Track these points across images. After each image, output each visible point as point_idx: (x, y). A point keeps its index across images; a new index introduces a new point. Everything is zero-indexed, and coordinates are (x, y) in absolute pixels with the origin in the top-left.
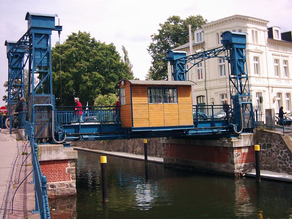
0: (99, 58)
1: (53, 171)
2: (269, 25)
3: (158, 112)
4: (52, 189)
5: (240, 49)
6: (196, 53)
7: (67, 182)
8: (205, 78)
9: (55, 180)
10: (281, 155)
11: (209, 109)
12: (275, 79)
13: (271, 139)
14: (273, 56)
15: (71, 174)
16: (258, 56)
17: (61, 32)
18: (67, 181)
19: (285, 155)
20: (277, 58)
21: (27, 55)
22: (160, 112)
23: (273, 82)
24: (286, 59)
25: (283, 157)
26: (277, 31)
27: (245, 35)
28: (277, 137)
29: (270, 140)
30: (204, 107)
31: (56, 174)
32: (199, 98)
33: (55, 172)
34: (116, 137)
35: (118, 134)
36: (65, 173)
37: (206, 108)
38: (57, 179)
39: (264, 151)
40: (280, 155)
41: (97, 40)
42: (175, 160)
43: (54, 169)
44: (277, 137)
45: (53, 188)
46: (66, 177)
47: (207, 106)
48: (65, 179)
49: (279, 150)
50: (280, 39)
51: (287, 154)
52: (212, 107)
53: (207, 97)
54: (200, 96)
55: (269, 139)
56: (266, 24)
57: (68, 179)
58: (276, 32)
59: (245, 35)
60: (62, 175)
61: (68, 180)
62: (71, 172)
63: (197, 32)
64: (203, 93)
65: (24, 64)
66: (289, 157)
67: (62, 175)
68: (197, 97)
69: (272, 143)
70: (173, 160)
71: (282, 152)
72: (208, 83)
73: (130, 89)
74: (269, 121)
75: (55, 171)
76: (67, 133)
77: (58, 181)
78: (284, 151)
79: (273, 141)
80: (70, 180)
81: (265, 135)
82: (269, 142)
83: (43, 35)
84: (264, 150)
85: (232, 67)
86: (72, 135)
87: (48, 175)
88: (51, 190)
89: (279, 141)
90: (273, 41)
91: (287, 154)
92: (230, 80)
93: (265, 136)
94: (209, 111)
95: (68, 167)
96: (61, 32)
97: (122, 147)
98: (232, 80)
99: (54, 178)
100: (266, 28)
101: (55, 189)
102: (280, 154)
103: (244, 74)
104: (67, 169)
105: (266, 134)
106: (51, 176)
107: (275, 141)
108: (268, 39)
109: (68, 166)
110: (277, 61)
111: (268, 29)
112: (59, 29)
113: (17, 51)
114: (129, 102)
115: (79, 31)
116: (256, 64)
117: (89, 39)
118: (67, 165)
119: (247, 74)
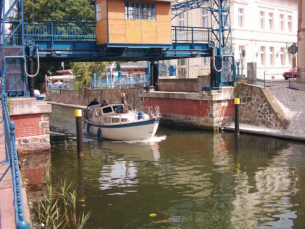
0: (75, 8)
4: (25, 144)
7: (40, 137)
10: (261, 108)
15: (45, 129)
18: (41, 136)
19: (265, 108)
25: (263, 111)
36: (39, 128)
39: (244, 105)
40: (259, 109)
43: (27, 123)
45: (26, 142)
46: (40, 131)
48: (38, 133)
49: (259, 104)
51: (267, 108)
55: (250, 93)
57: (41, 133)
60: (35, 130)
61: (42, 135)
62: (44, 126)
67: (35, 130)
71: (262, 106)
77: (31, 136)
80: (44, 134)
81: (246, 88)
84: (244, 103)
87: (20, 130)
88: (24, 145)
89: (259, 95)
91: (267, 108)
95: (41, 122)
99: (27, 132)
101: (28, 144)
102: (260, 107)
104: (40, 123)
105: (247, 87)
107: (255, 95)
109: (42, 120)
110: (262, 13)
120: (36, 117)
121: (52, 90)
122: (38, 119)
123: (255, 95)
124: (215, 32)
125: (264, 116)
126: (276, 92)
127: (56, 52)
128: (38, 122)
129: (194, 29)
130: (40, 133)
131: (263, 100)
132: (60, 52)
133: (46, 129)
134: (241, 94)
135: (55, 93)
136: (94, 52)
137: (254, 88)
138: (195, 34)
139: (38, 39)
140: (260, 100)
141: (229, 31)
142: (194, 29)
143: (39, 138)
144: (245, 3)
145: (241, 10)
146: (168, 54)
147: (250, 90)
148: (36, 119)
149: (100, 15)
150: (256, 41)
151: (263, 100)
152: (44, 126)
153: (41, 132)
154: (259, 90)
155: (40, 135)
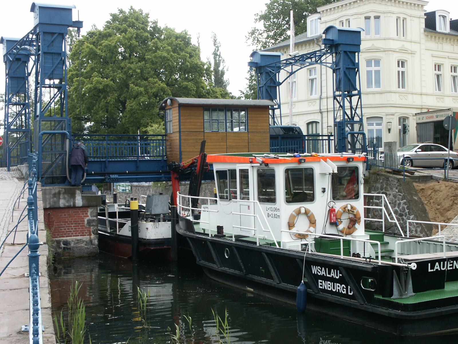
0: (165, 54)
1: (67, 222)
2: (429, 9)
3: (218, 144)
5: (350, 52)
7: (86, 238)
8: (320, 94)
9: (69, 234)
10: (399, 208)
11: (324, 141)
12: (435, 96)
13: (387, 185)
15: (92, 227)
16: (406, 59)
17: (81, 29)
19: (403, 208)
20: (439, 61)
21: (34, 59)
22: (222, 144)
25: (400, 211)
26: (444, 17)
27: (360, 32)
28: (395, 181)
29: (386, 188)
30: (318, 138)
31: (71, 226)
32: (310, 126)
33: (69, 224)
34: (159, 177)
35: (161, 174)
36: (84, 226)
37: (321, 139)
38: (73, 234)
39: (378, 203)
40: (397, 208)
41: (161, 25)
43: (69, 219)
44: (395, 181)
46: (85, 231)
47: (322, 136)
48: (84, 233)
49: (395, 202)
50: (448, 30)
51: (406, 206)
52: (329, 138)
53: (322, 123)
54: (312, 123)
55: (385, 186)
56: (422, 6)
58: (442, 18)
59: (360, 32)
60: (80, 228)
62: (92, 224)
63: (311, 19)
64: (317, 118)
65: (29, 71)
66: (407, 211)
67: (80, 228)
68: (308, 124)
69: (388, 191)
71: (399, 204)
73: (178, 111)
74: (389, 160)
75: (70, 222)
76: (87, 170)
77: (74, 236)
78: (401, 202)
79: (389, 189)
81: (380, 180)
82: (385, 190)
83: (56, 35)
84: (377, 201)
85: (338, 80)
86: (96, 174)
89: (397, 189)
90: (437, 35)
91: (406, 206)
92: (335, 98)
93: (379, 181)
94: (324, 144)
95: (88, 218)
96: (81, 29)
98: (338, 98)
100: (423, 14)
102: (397, 206)
103: (355, 89)
104: (86, 220)
105: (382, 178)
106: (64, 229)
107: (392, 189)
108: (425, 31)
109: (88, 216)
110: (438, 67)
112: (79, 25)
113: (19, 53)
114: (177, 128)
115: (131, 7)
117: (148, 22)
118: (87, 214)
119: (359, 90)
120: (81, 212)
121: (119, 186)
122: (83, 214)
123: (392, 189)
124: (338, 98)
125: (402, 219)
128: (83, 219)
130: (86, 233)
131: (401, 196)
133: (93, 228)
134: (374, 188)
135: (123, 190)
137: (390, 179)
140: (398, 196)
141: (358, 96)
143: (84, 239)
144: (382, 50)
145: (402, 63)
147: (385, 181)
148: (80, 214)
151: (401, 196)
152: (92, 224)
153: (86, 232)
154: (396, 181)
155: (85, 235)
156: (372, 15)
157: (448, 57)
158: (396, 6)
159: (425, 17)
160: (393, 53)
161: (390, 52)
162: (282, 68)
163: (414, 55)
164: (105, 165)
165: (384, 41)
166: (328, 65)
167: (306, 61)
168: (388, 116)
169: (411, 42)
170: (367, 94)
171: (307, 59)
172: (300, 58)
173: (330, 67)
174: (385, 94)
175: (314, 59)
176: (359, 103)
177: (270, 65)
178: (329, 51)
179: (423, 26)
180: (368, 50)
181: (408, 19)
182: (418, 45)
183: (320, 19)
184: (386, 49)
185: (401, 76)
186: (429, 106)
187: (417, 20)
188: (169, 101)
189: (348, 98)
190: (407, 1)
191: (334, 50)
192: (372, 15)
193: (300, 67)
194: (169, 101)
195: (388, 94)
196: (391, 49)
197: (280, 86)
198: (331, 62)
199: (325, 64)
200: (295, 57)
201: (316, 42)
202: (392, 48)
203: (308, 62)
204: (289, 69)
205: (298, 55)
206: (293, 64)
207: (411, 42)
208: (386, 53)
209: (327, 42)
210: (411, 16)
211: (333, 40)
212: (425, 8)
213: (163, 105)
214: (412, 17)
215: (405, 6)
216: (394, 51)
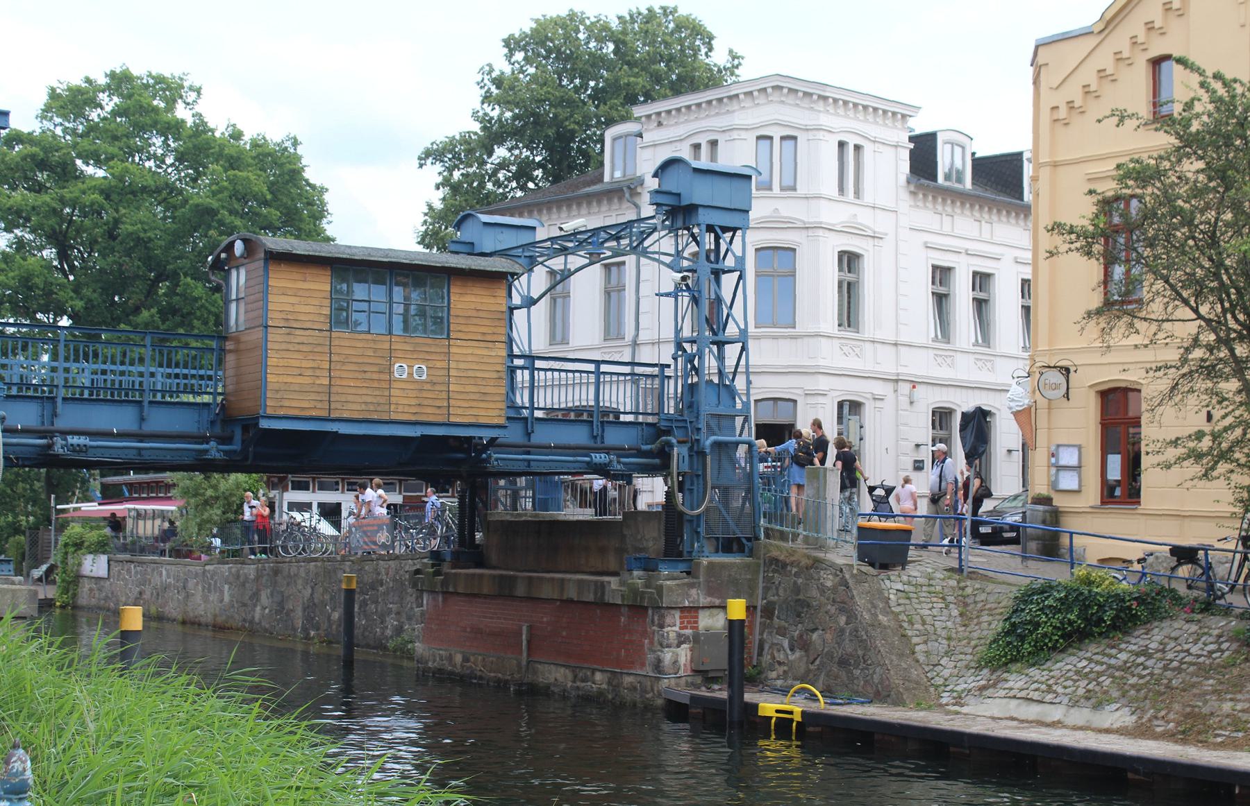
2: (921, 126)
6: (563, 233)
14: (929, 250)
20: (944, 260)
23: (919, 364)
24: (984, 266)
42: (458, 658)
70: (450, 658)
72: (333, 380)
97: (264, 608)
100: (904, 137)
108: (908, 182)
111: (911, 139)
116: (849, 284)
126: (900, 586)
127: (69, 438)
129: (604, 368)
132: (82, 440)
136: (213, 444)
138: (607, 387)
139: (159, 395)
142: (604, 368)
144: (800, 225)
146: (497, 460)
149: (242, 310)
150: (914, 384)
156: (777, 133)
157: (967, 250)
158: (837, 115)
159: (912, 146)
160: (827, 233)
161: (820, 232)
162: (540, 259)
163: (881, 243)
164: (55, 408)
165: (805, 201)
166: (663, 258)
167: (606, 245)
168: (809, 398)
169: (873, 342)
170: (757, 338)
171: (606, 241)
172: (589, 237)
173: (668, 266)
174: (806, 340)
175: (625, 242)
176: (743, 362)
177: (512, 252)
178: (667, 223)
179: (905, 167)
180: (768, 225)
181: (868, 149)
182: (894, 214)
183: (640, 136)
184: (809, 223)
185: (849, 293)
186: (916, 376)
187: (890, 152)
188: (239, 247)
189: (715, 348)
190: (865, 103)
191: (680, 223)
192: (777, 133)
193: (587, 261)
194: (239, 247)
195: (812, 340)
196: (821, 223)
197: (533, 308)
198: (673, 252)
199: (656, 256)
200: (575, 234)
201: (627, 195)
202: (824, 220)
203: (609, 249)
204: (557, 263)
205: (583, 229)
206: (570, 251)
207: (873, 342)
208: (810, 233)
209: (662, 199)
210: (874, 142)
211: (679, 195)
212: (911, 123)
213: (223, 255)
214: (877, 145)
215: (861, 116)
216: (830, 230)
